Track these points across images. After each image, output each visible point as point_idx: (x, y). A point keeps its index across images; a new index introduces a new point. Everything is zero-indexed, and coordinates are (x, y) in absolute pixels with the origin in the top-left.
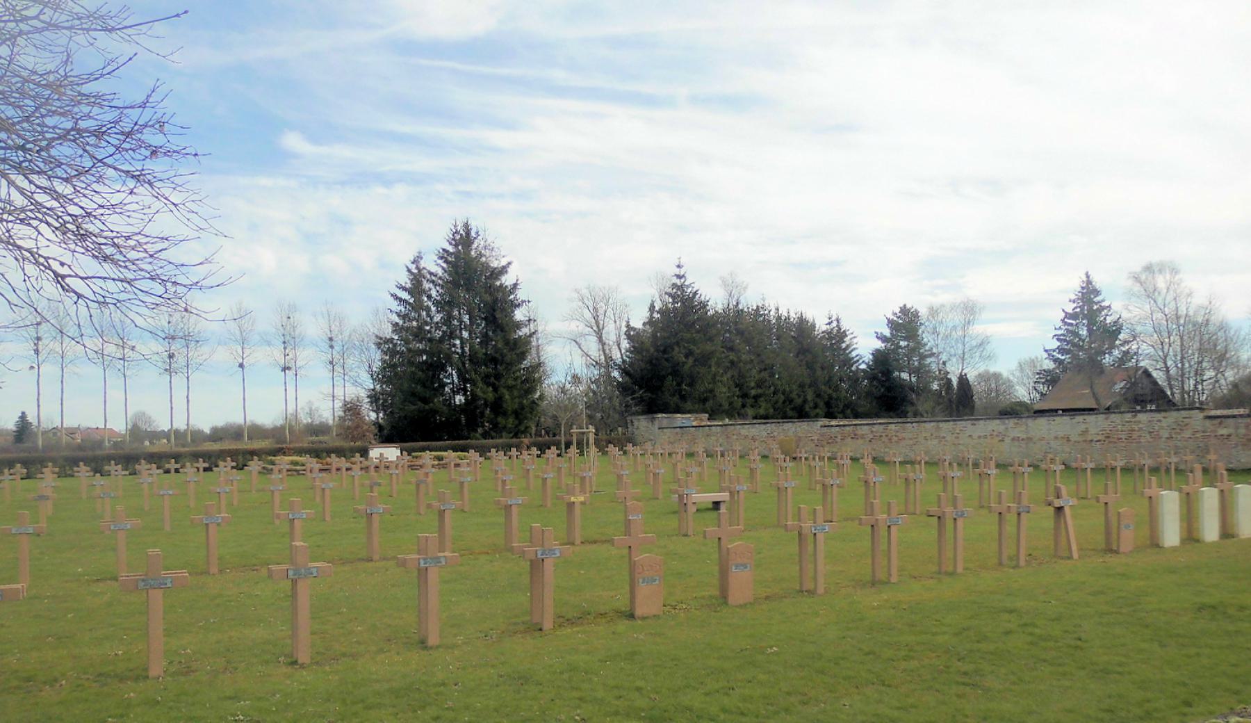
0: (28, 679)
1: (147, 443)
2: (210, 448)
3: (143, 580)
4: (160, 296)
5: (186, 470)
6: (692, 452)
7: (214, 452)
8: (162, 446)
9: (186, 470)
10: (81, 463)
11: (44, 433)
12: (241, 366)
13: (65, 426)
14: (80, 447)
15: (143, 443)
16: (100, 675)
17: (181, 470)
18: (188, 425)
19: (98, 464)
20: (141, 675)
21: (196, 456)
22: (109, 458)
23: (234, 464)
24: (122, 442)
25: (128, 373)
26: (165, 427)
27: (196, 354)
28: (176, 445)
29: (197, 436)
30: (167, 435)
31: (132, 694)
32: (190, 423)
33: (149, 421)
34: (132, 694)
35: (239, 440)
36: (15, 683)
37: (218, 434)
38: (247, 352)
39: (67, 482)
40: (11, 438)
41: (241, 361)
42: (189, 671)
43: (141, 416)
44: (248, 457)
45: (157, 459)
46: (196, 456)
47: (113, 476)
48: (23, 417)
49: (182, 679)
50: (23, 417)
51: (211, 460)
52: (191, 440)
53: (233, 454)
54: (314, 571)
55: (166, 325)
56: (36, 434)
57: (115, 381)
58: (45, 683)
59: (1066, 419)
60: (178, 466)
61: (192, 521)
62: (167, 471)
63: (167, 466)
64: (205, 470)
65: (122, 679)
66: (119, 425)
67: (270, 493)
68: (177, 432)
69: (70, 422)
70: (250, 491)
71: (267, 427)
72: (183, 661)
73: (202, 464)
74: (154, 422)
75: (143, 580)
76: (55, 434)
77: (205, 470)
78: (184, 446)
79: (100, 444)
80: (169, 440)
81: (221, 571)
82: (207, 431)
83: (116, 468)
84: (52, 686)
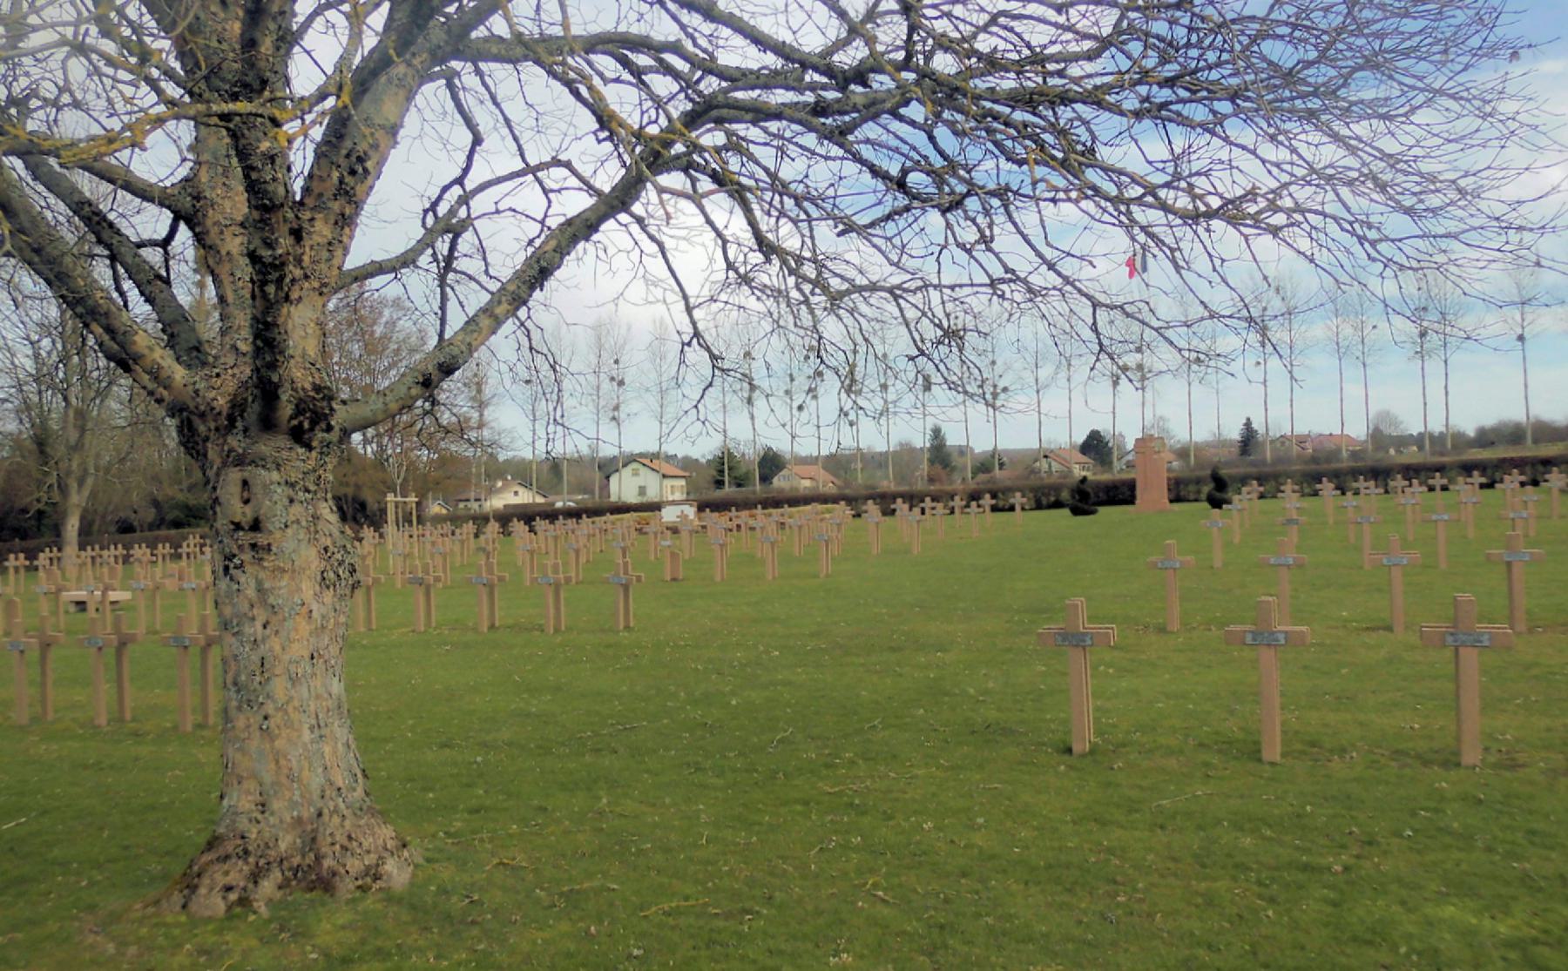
0: (1313, 744)
1: (1392, 451)
2: (1479, 457)
3: (1452, 634)
4: (1499, 250)
5: (1457, 488)
6: (34, 447)
7: (1490, 461)
8: (1412, 455)
9: (1457, 488)
10: (1324, 479)
11: (1272, 442)
12: (1521, 338)
13: (1429, 428)
14: (1314, 459)
15: (1387, 452)
16: (1397, 752)
17: (1451, 487)
18: (1447, 425)
19: (1343, 480)
20: (1451, 761)
21: (1467, 468)
22: (1355, 473)
23: (1523, 478)
24: (1363, 451)
25: (1368, 361)
26: (1415, 428)
27: (91, 341)
28: (1433, 453)
29: (1460, 441)
30: (1419, 440)
31: (1444, 784)
32: (1450, 422)
33: (1395, 422)
34: (1444, 784)
35: (1519, 444)
36: (1299, 746)
37: (1485, 438)
38: (1529, 318)
39: (1308, 503)
40: (1236, 450)
41: (1519, 331)
42: (1514, 766)
43: (1385, 416)
44: (1541, 468)
45: (1411, 472)
46: (1467, 468)
47: (1362, 495)
48: (1248, 424)
49: (1508, 774)
50: (1248, 424)
51: (1491, 474)
52: (1453, 446)
53: (1519, 464)
54: (1281, 637)
55: (1416, 292)
56: (1263, 444)
57: (1353, 372)
58: (1331, 751)
59: (379, 257)
60: (1445, 481)
61: (1488, 556)
62: (1431, 489)
63: (1431, 482)
64: (1482, 486)
65: (1426, 763)
66: (1358, 430)
67: (1510, 522)
68: (1431, 436)
69: (1301, 429)
70: (1549, 517)
71: (1558, 424)
72: (1503, 749)
73: (1478, 478)
74: (1401, 423)
75: (1452, 634)
76: (1283, 443)
77: (1482, 486)
78: (1442, 454)
79: (1334, 455)
80: (1421, 448)
81: (1531, 631)
82: (1471, 432)
83: (1366, 484)
84: (1341, 757)
